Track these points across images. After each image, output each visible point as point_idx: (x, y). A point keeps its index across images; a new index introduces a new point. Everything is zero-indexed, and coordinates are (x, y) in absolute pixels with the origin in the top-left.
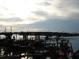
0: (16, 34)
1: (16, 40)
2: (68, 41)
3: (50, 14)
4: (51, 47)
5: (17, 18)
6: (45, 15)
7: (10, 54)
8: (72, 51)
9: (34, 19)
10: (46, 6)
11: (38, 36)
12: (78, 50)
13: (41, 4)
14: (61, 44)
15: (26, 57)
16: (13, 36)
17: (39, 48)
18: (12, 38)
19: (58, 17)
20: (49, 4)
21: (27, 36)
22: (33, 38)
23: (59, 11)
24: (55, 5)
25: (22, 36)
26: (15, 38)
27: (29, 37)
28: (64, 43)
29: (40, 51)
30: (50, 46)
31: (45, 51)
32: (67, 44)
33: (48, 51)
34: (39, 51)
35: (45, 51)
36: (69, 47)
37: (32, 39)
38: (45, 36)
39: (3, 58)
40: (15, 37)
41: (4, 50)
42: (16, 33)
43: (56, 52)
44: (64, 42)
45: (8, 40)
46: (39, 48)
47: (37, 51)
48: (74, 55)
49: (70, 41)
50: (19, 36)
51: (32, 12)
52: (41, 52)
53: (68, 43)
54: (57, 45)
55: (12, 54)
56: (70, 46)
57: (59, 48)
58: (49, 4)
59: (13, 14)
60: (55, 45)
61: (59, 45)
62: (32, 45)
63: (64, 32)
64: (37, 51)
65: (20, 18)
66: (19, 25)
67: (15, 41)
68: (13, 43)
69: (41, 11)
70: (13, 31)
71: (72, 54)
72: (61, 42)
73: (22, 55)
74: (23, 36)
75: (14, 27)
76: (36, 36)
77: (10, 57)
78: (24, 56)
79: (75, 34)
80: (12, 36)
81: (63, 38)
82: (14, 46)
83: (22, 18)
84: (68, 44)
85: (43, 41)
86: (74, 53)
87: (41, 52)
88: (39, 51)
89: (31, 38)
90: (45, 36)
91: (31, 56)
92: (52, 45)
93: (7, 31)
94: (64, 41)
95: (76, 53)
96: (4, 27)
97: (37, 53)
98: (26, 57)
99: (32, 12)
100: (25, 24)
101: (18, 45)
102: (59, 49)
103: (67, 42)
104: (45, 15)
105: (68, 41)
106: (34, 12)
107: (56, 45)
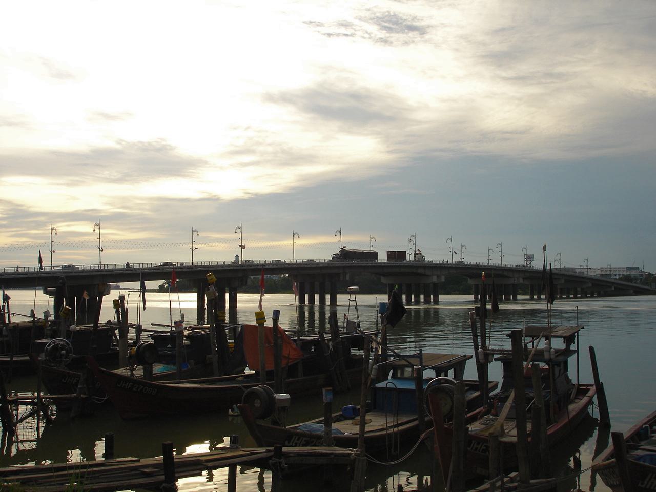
0: (137, 285)
1: (139, 329)
2: (569, 339)
3: (420, 116)
4: (439, 388)
5: (146, 148)
6: (390, 119)
7: (88, 453)
8: (605, 424)
9: (291, 158)
10: (385, 41)
11: (322, 300)
12: (654, 410)
13: (346, 25)
14: (510, 362)
15: (221, 474)
16: (114, 295)
17: (327, 396)
18: (107, 313)
19: (485, 136)
20: (412, 28)
21: (233, 301)
22: (276, 313)
23: (510, 90)
24: (464, 37)
25: (188, 301)
26: (132, 319)
27: (247, 302)
28: (539, 355)
29: (338, 420)
30: (418, 378)
31: (376, 423)
32: (559, 360)
33: (407, 422)
34: (327, 423)
35: (376, 423)
36: (582, 391)
37: (269, 323)
38: (384, 298)
39: (36, 482)
40: (132, 301)
41: (39, 408)
42: (129, 274)
43: (474, 427)
44: (542, 344)
45: (69, 334)
46: (327, 396)
47: (314, 425)
48: (618, 453)
49: (583, 343)
50: (165, 296)
51: (270, 98)
52: (348, 429)
53: (568, 352)
54: (482, 369)
55: (100, 448)
56: (587, 378)
57: (502, 399)
58: (412, 28)
59: (107, 116)
60: (459, 372)
61: (496, 372)
62: (270, 375)
63: (537, 265)
64: (314, 425)
65: (172, 148)
66: (165, 204)
67: (132, 334)
68: (114, 359)
69: (344, 86)
70: (114, 259)
71: (601, 446)
72: (508, 345)
73: (563, 296)
74: (200, 300)
75: (117, 219)
76: (302, 300)
77: (87, 471)
78: (195, 466)
79: (627, 278)
80: (108, 302)
81: (533, 312)
82: (121, 378)
83: (184, 148)
84: (572, 360)
85: (361, 341)
86: (617, 436)
87: (348, 429)
88: (327, 423)
89: (260, 316)
90: (384, 298)
91: (263, 464)
92: (439, 370)
93: (59, 260)
94: (535, 334)
95: (640, 435)
96: (38, 225)
97: (311, 439)
98: (221, 474)
99: (270, 98)
100: (215, 199)
101: (158, 369)
102: (492, 405)
103: (558, 344)
104: (390, 119)
105: (569, 339)
106: (285, 98)
107: (471, 373)
